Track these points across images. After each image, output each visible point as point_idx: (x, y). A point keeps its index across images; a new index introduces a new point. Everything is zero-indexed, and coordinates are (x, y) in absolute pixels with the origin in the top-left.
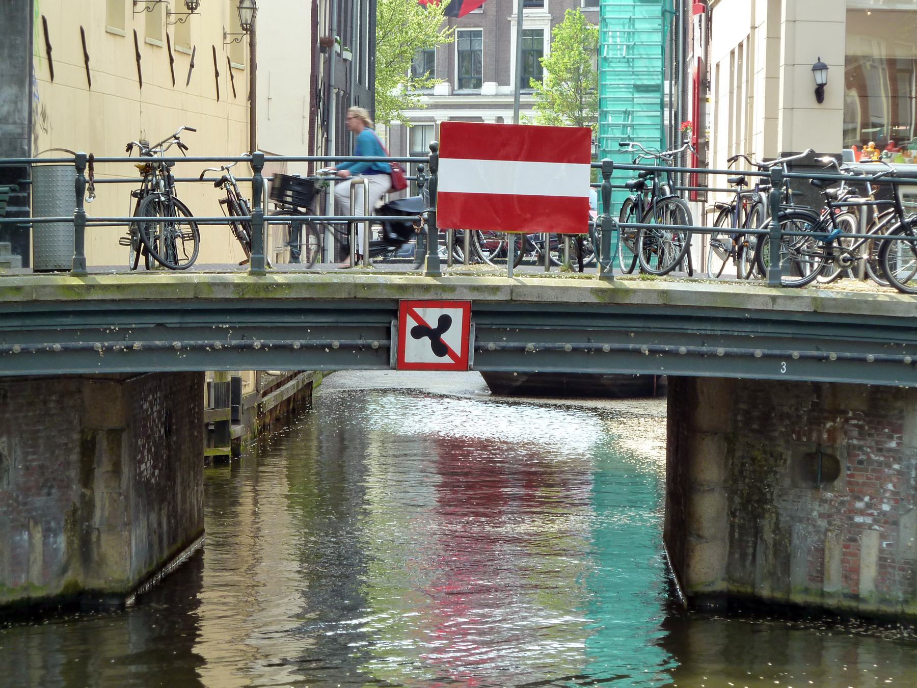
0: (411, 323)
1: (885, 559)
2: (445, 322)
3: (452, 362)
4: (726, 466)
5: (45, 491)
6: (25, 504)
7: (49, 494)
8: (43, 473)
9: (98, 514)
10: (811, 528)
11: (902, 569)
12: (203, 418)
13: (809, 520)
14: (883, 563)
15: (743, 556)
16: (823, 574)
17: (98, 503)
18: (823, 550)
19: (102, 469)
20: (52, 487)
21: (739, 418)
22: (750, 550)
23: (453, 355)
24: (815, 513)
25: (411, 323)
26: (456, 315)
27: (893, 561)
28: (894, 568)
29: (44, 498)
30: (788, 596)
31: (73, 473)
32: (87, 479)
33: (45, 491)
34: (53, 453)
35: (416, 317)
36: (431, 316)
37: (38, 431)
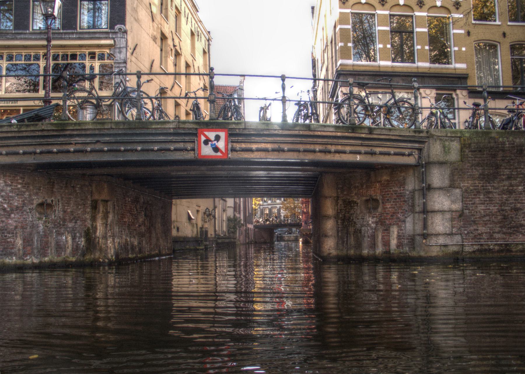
0: (203, 138)
1: (400, 236)
2: (218, 138)
3: (221, 155)
4: (335, 209)
5: (74, 221)
6: (64, 225)
7: (76, 223)
8: (73, 214)
9: (98, 231)
10: (369, 228)
11: (408, 239)
12: (171, 216)
13: (369, 225)
14: (399, 237)
15: (343, 242)
16: (375, 244)
17: (98, 228)
18: (374, 235)
19: (100, 216)
20: (77, 220)
21: (339, 221)
22: (346, 239)
23: (222, 152)
24: (370, 222)
25: (203, 138)
26: (222, 134)
27: (404, 236)
28: (404, 239)
29: (74, 224)
30: (361, 252)
31: (88, 216)
32: (94, 219)
33: (74, 221)
34: (78, 207)
35: (205, 136)
36: (212, 135)
37: (70, 198)
